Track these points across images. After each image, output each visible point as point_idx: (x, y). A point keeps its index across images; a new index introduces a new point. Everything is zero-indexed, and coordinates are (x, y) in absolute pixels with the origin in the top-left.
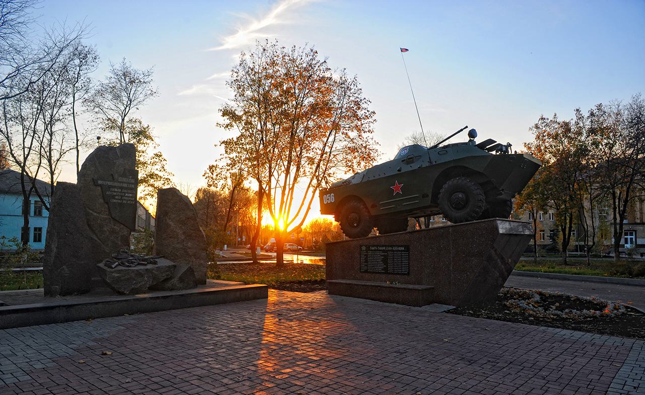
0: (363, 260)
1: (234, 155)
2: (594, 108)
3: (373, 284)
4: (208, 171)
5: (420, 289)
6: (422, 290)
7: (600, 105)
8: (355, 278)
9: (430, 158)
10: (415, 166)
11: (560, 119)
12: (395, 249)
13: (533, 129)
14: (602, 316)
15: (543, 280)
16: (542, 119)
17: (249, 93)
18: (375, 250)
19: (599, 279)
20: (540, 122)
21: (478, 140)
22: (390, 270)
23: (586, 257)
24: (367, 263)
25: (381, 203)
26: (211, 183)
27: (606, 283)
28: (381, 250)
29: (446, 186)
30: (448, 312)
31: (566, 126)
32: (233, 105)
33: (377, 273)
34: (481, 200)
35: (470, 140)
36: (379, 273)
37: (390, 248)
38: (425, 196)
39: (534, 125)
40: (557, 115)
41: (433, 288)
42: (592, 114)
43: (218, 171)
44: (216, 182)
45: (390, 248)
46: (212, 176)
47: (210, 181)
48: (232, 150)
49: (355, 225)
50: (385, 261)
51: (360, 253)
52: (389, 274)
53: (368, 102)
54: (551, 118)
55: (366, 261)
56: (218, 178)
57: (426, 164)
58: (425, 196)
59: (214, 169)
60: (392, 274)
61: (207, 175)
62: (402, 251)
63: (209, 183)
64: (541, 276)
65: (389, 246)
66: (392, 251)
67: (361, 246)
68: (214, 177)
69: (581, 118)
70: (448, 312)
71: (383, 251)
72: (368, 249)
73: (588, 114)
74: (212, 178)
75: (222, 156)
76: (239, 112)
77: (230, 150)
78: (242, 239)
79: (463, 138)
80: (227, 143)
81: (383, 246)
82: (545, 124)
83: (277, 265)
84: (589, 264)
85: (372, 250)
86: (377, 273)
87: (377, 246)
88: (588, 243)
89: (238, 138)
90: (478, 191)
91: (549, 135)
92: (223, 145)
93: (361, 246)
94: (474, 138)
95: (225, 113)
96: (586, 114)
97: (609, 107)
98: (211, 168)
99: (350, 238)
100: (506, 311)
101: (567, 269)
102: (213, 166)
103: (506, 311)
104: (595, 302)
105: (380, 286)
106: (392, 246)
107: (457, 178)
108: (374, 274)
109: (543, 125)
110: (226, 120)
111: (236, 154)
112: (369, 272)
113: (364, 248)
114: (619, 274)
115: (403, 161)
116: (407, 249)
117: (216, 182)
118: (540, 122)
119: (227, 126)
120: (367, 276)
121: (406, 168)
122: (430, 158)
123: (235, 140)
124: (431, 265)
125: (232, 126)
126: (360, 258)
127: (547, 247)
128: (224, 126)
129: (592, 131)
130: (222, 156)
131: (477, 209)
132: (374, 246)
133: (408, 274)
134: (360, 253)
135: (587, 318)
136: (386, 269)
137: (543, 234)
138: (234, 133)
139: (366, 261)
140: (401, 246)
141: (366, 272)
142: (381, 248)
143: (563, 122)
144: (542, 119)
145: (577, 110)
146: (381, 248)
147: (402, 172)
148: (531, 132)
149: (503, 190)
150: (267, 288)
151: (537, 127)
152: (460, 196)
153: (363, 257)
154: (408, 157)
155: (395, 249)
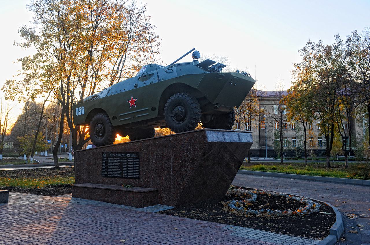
0: (104, 165)
1: (30, 72)
2: (351, 34)
3: (106, 188)
4: (6, 85)
5: (142, 191)
6: (144, 193)
7: (356, 32)
8: (98, 183)
9: (158, 75)
10: (148, 82)
11: (325, 44)
12: (128, 155)
13: (302, 51)
14: (292, 215)
15: (294, 181)
16: (309, 42)
17: (47, 17)
18: (113, 157)
19: (339, 180)
20: (308, 45)
21: (200, 61)
22: (125, 175)
23: (344, 160)
24: (107, 168)
25: (120, 115)
26: (9, 96)
27: (345, 183)
28: (117, 157)
29: (170, 100)
30: (165, 212)
31: (328, 51)
32: (29, 26)
33: (114, 177)
34: (196, 113)
35: (194, 61)
36: (116, 177)
37: (125, 155)
38: (153, 109)
39: (302, 48)
40: (322, 40)
41: (157, 191)
42: (349, 40)
43: (16, 85)
44: (13, 95)
45: (125, 155)
46: (10, 90)
47: (7, 94)
48: (29, 67)
49: (101, 134)
50: (121, 167)
51: (102, 159)
52: (124, 178)
53: (154, 27)
54: (317, 42)
55: (107, 167)
56: (15, 92)
57: (156, 81)
58: (153, 109)
59: (12, 84)
60: (126, 178)
61: (4, 89)
62: (134, 158)
63: (6, 96)
64: (294, 178)
65: (124, 153)
66: (126, 157)
67: (103, 153)
68: (12, 91)
69: (340, 42)
70: (165, 212)
71: (120, 158)
72: (108, 157)
73: (346, 40)
74: (10, 92)
75: (19, 72)
76: (38, 33)
77: (26, 66)
78: (64, 146)
79: (189, 59)
80: (25, 61)
81: (120, 153)
82: (312, 47)
83: (74, 170)
84: (347, 167)
85: (111, 157)
86: (114, 177)
87: (115, 153)
88: (346, 148)
89: (34, 57)
90: (194, 105)
91: (315, 57)
92: (20, 63)
93: (103, 153)
94: (198, 58)
95: (24, 33)
96: (344, 39)
97: (366, 33)
98: (8, 83)
99: (96, 146)
100: (214, 211)
101: (330, 171)
102: (10, 81)
103: (214, 211)
104: (301, 202)
105: (111, 189)
106: (126, 153)
107: (178, 94)
108: (113, 179)
109: (311, 48)
110: (24, 40)
111: (32, 71)
112: (109, 177)
113: (105, 155)
114: (357, 176)
115: (139, 78)
116: (138, 156)
117: (13, 95)
118: (308, 45)
119: (25, 45)
120: (107, 180)
121: (141, 84)
122: (158, 75)
123: (32, 58)
124: (156, 170)
125: (28, 45)
126: (102, 164)
127: (322, 152)
128: (22, 45)
129: (349, 54)
130: (19, 72)
131: (193, 121)
132: (112, 153)
133: (139, 178)
134: (102, 159)
135: (279, 217)
136: (121, 174)
137: (295, 141)
138: (32, 50)
139: (107, 167)
140: (134, 153)
141: (106, 176)
142: (118, 155)
143: (328, 46)
144: (309, 42)
145: (337, 36)
146: (118, 155)
147: (138, 87)
148: (300, 54)
149: (217, 104)
150: (7, 192)
151: (305, 50)
152: (180, 109)
153: (104, 163)
154: (143, 75)
155: (128, 155)
